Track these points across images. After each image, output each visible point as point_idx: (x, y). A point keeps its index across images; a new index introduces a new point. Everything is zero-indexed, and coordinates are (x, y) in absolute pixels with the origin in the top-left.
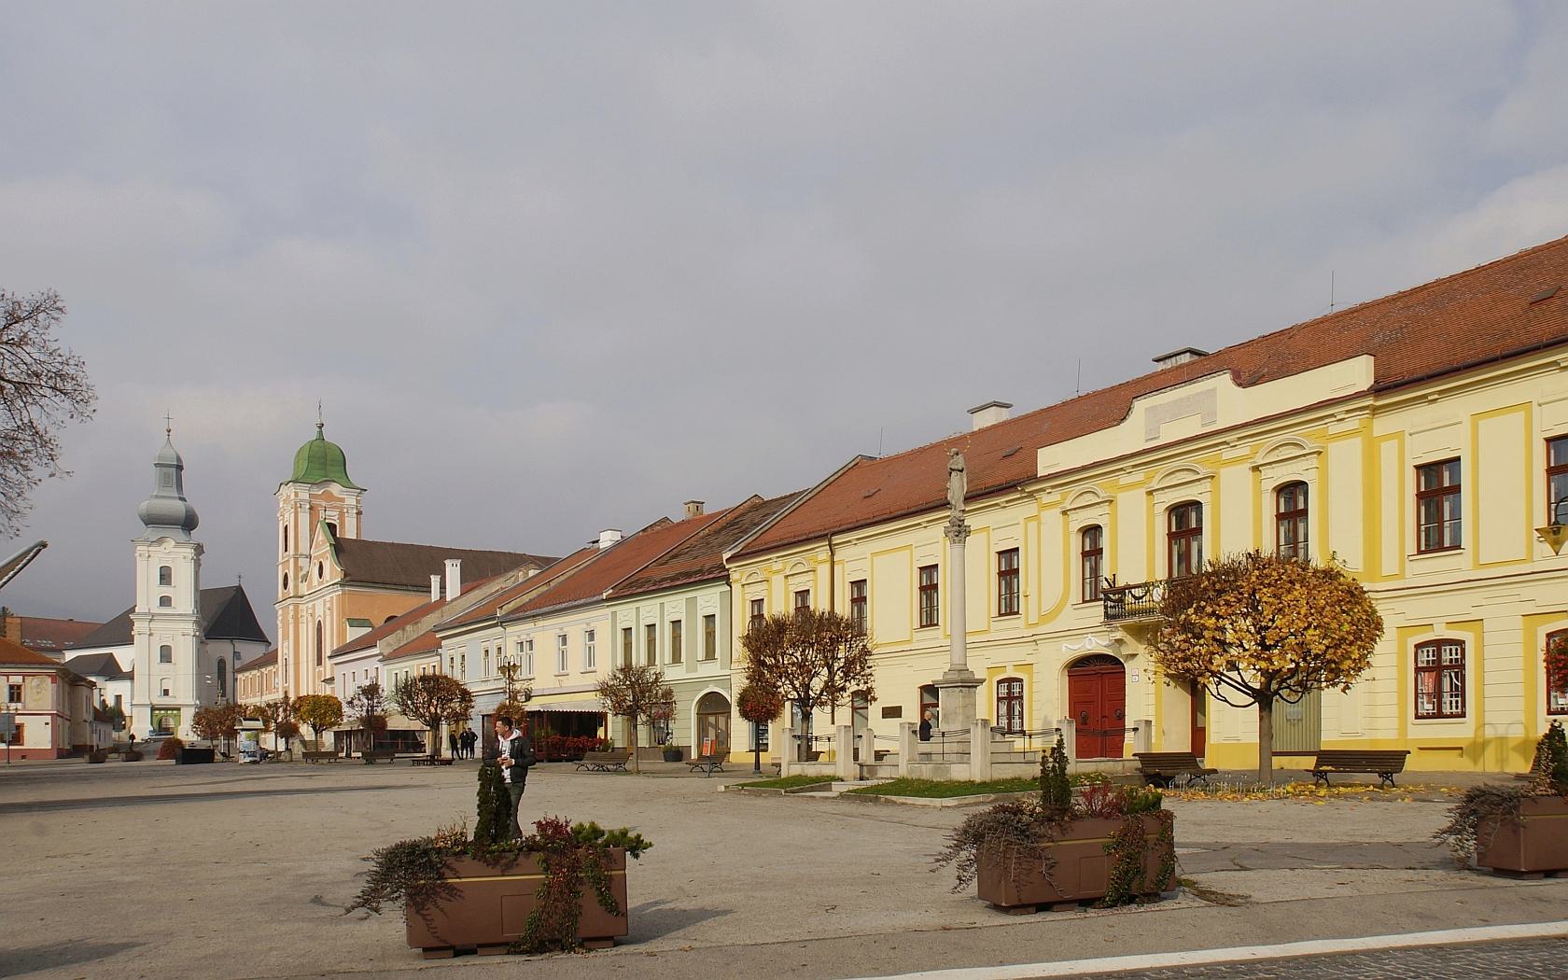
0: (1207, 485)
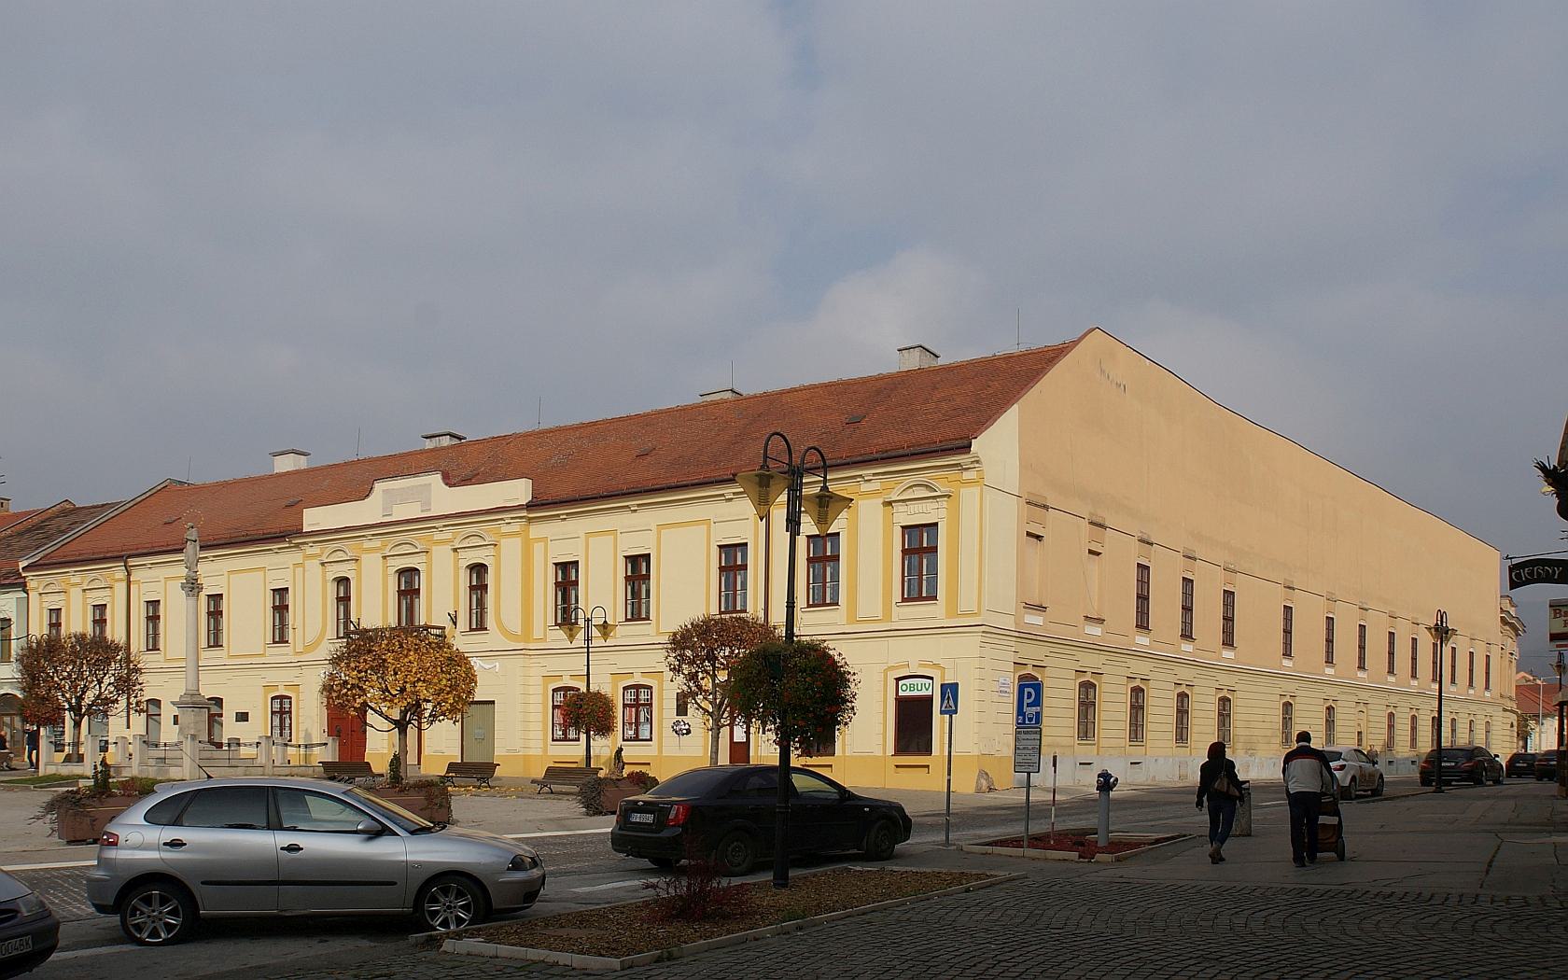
0: (423, 558)
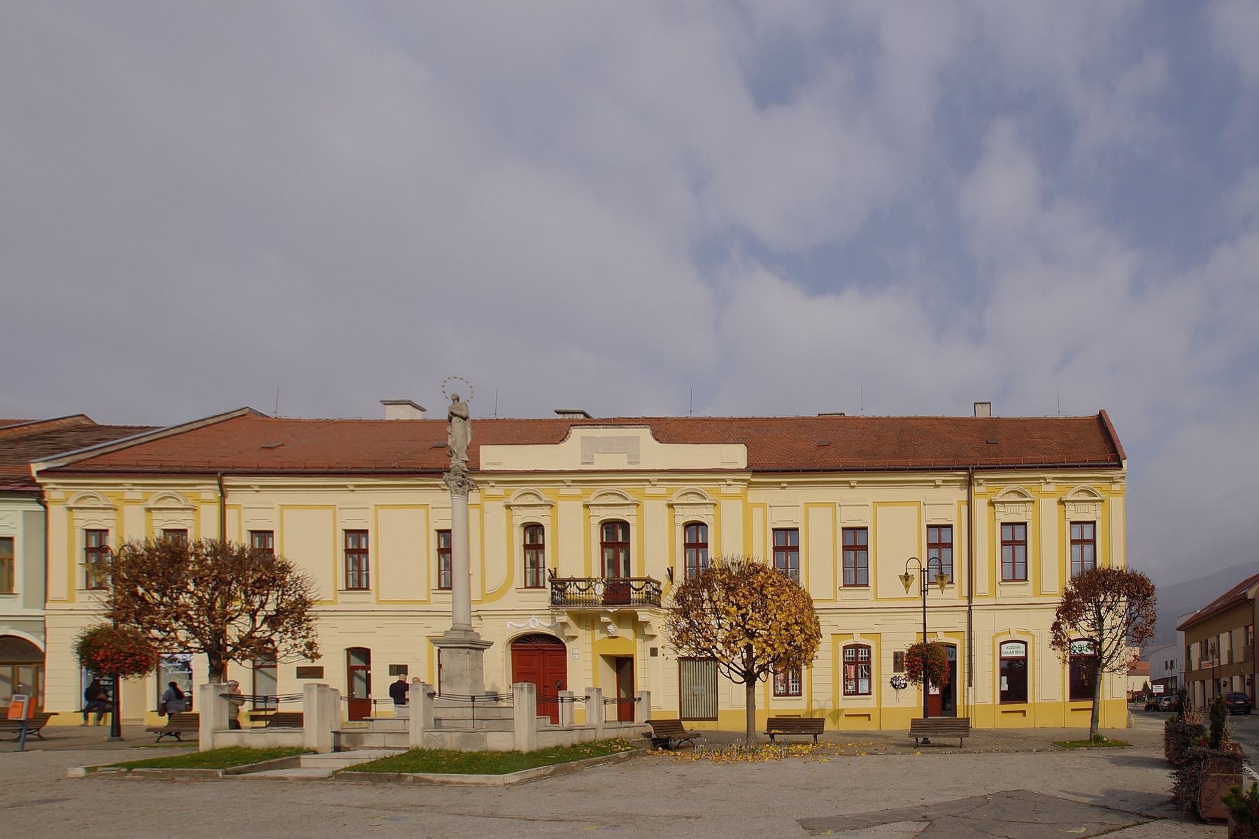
0: (633, 510)
